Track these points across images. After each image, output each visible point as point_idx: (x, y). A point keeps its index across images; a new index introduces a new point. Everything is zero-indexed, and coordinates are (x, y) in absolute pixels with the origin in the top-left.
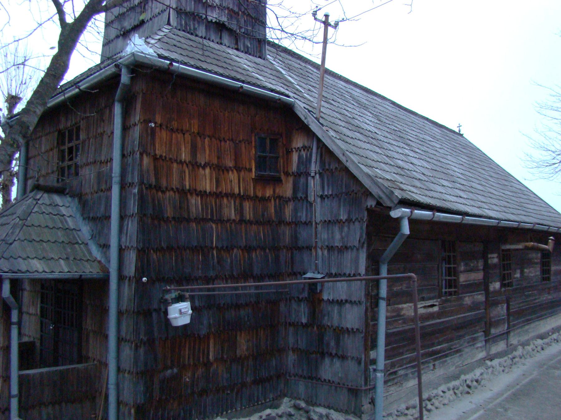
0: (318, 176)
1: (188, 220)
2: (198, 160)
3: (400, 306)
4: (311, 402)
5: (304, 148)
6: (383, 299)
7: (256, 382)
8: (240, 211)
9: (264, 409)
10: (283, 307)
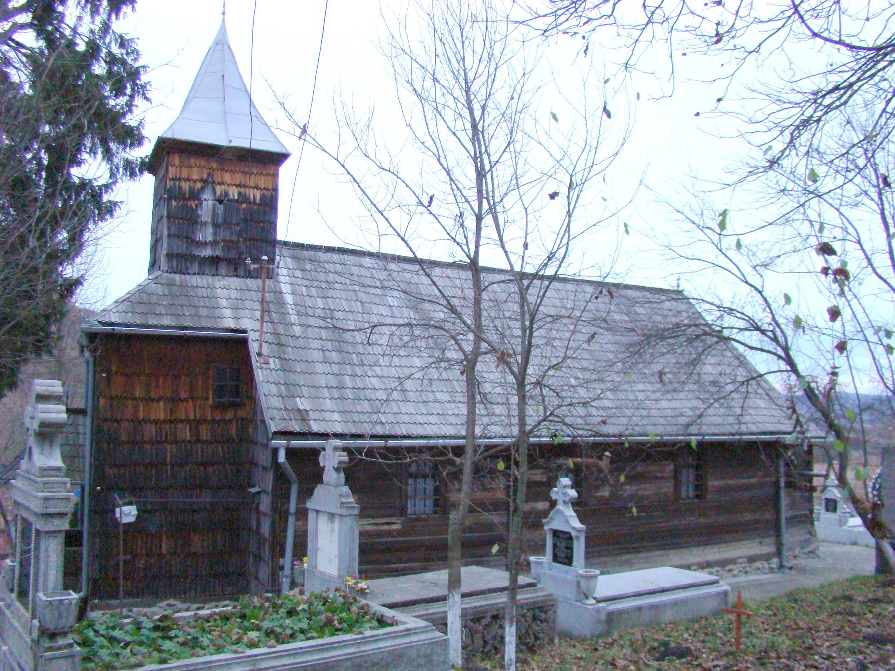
8: (196, 434)
9: (225, 600)
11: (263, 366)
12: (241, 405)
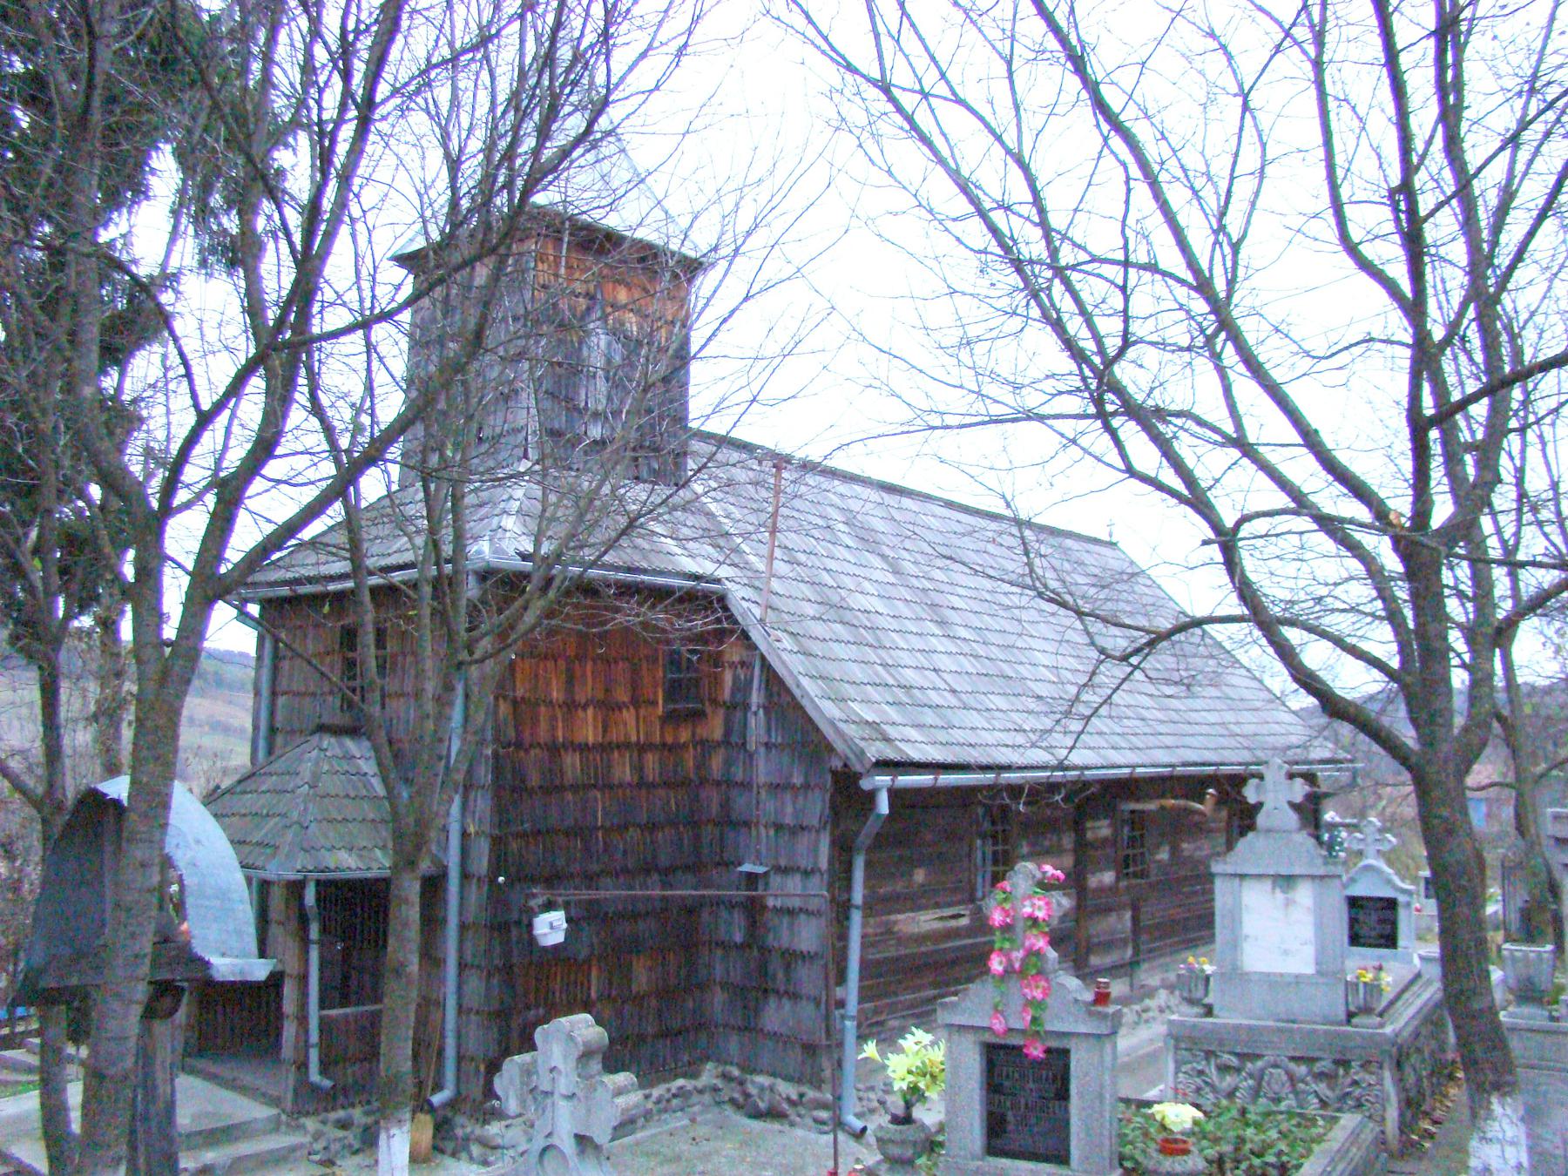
0: (761, 712)
1: (561, 789)
2: (577, 698)
3: (893, 917)
4: (749, 1068)
5: (743, 664)
6: (857, 907)
7: (665, 1034)
8: (639, 769)
9: (676, 1077)
10: (705, 916)
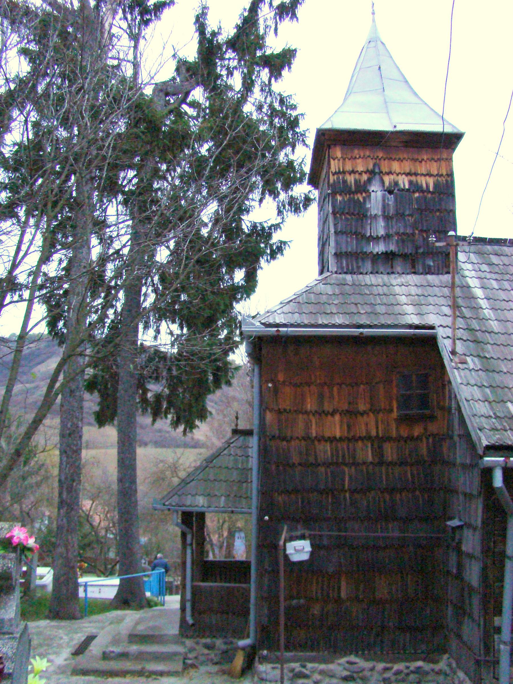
7: (403, 629)
8: (379, 452)
9: (417, 660)
11: (460, 365)
12: (432, 418)
